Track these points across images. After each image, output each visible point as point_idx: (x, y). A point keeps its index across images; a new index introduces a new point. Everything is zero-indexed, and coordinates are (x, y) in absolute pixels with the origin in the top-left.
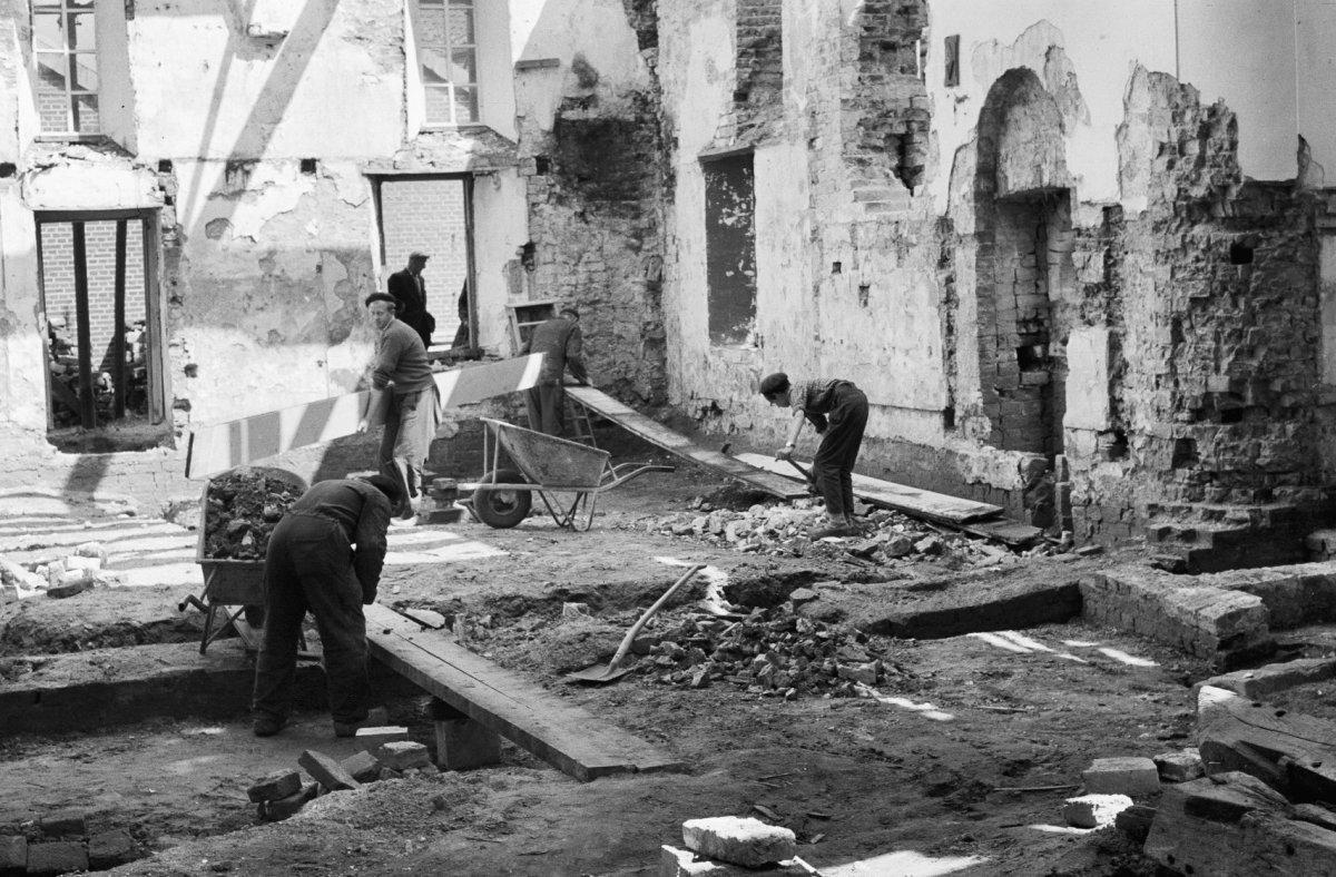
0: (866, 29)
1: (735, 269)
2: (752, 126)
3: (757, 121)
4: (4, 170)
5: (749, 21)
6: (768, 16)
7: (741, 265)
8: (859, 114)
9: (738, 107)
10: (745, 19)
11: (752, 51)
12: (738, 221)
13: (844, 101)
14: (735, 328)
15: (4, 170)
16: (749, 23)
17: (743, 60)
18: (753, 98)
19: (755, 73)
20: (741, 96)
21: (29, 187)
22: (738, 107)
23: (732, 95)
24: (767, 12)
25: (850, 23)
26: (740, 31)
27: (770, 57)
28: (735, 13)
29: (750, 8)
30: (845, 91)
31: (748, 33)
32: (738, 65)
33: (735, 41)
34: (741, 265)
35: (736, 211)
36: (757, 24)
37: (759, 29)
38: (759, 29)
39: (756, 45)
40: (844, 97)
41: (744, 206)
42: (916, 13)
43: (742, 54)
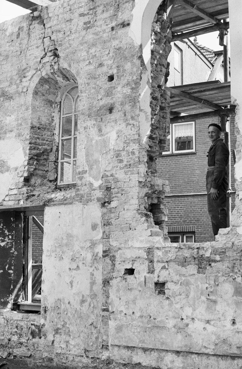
0: (150, 147)
1: (4, 269)
2: (33, 195)
3: (36, 193)
4: (199, 368)
5: (35, 142)
6: (45, 142)
7: (7, 267)
8: (146, 190)
9: (25, 185)
10: (33, 141)
11: (36, 157)
12: (7, 244)
13: (140, 182)
14: (2, 300)
15: (199, 368)
16: (35, 143)
17: (31, 162)
18: (33, 181)
19: (35, 169)
20: (27, 180)
21: (190, 345)
22: (25, 185)
23: (22, 179)
24: (44, 140)
25: (144, 142)
26: (31, 147)
27: (42, 162)
28: (28, 137)
29: (36, 136)
30: (141, 177)
31: (34, 149)
32: (28, 164)
33: (28, 152)
34: (7, 267)
35: (6, 239)
36: (39, 144)
37: (40, 147)
38: (40, 147)
39: (38, 155)
40: (140, 180)
41: (10, 237)
42: (165, 143)
43: (31, 159)
